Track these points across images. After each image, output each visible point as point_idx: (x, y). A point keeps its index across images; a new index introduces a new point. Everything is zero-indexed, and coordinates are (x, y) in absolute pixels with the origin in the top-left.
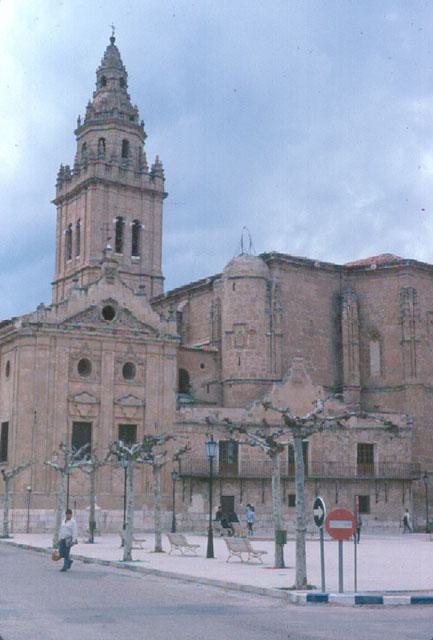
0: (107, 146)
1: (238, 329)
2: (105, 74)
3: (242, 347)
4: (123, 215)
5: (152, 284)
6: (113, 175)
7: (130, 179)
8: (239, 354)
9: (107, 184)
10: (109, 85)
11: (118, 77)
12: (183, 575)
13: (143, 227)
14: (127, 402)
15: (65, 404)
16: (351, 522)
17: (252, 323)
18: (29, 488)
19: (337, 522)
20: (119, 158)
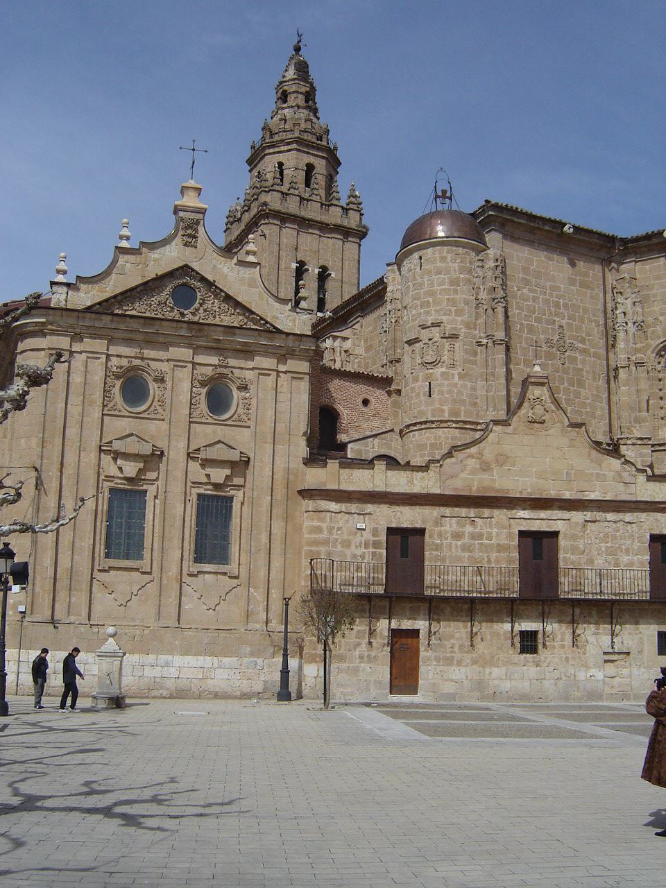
0: (285, 172)
1: (425, 335)
2: (285, 88)
3: (433, 364)
4: (306, 259)
5: (573, 610)
6: (292, 206)
7: (312, 212)
8: (428, 377)
9: (284, 218)
10: (292, 100)
11: (303, 90)
12: (359, 707)
13: (333, 275)
14: (212, 453)
15: (93, 456)
16: (126, 702)
17: (451, 322)
18: (22, 608)
19: (263, 359)
20: (302, 186)
